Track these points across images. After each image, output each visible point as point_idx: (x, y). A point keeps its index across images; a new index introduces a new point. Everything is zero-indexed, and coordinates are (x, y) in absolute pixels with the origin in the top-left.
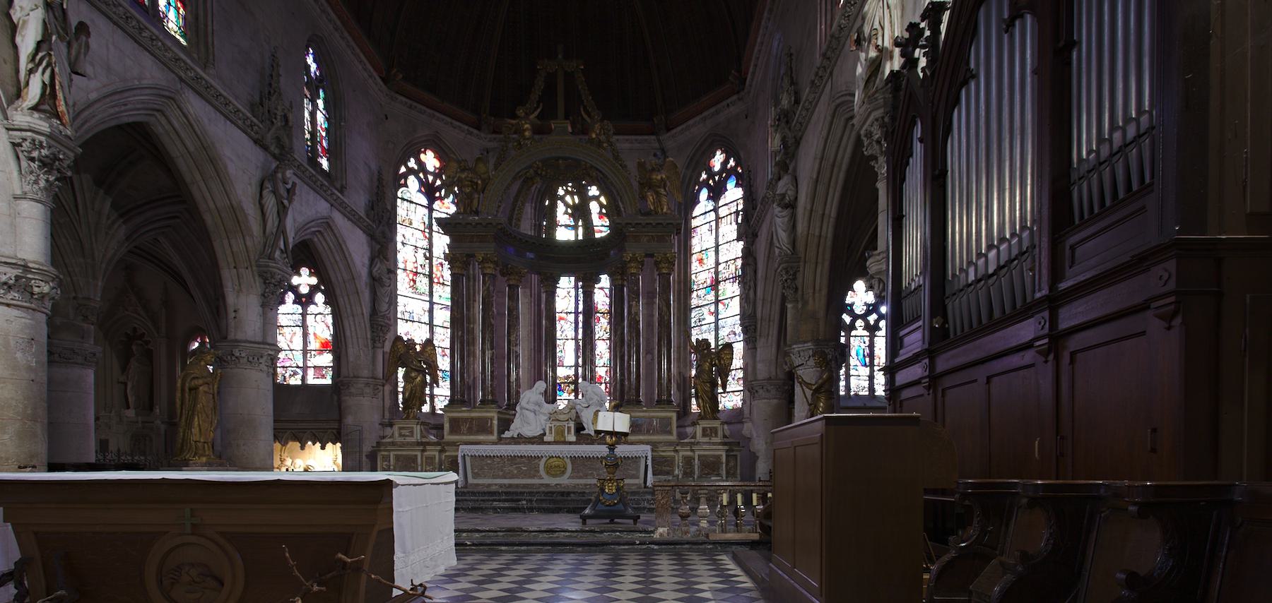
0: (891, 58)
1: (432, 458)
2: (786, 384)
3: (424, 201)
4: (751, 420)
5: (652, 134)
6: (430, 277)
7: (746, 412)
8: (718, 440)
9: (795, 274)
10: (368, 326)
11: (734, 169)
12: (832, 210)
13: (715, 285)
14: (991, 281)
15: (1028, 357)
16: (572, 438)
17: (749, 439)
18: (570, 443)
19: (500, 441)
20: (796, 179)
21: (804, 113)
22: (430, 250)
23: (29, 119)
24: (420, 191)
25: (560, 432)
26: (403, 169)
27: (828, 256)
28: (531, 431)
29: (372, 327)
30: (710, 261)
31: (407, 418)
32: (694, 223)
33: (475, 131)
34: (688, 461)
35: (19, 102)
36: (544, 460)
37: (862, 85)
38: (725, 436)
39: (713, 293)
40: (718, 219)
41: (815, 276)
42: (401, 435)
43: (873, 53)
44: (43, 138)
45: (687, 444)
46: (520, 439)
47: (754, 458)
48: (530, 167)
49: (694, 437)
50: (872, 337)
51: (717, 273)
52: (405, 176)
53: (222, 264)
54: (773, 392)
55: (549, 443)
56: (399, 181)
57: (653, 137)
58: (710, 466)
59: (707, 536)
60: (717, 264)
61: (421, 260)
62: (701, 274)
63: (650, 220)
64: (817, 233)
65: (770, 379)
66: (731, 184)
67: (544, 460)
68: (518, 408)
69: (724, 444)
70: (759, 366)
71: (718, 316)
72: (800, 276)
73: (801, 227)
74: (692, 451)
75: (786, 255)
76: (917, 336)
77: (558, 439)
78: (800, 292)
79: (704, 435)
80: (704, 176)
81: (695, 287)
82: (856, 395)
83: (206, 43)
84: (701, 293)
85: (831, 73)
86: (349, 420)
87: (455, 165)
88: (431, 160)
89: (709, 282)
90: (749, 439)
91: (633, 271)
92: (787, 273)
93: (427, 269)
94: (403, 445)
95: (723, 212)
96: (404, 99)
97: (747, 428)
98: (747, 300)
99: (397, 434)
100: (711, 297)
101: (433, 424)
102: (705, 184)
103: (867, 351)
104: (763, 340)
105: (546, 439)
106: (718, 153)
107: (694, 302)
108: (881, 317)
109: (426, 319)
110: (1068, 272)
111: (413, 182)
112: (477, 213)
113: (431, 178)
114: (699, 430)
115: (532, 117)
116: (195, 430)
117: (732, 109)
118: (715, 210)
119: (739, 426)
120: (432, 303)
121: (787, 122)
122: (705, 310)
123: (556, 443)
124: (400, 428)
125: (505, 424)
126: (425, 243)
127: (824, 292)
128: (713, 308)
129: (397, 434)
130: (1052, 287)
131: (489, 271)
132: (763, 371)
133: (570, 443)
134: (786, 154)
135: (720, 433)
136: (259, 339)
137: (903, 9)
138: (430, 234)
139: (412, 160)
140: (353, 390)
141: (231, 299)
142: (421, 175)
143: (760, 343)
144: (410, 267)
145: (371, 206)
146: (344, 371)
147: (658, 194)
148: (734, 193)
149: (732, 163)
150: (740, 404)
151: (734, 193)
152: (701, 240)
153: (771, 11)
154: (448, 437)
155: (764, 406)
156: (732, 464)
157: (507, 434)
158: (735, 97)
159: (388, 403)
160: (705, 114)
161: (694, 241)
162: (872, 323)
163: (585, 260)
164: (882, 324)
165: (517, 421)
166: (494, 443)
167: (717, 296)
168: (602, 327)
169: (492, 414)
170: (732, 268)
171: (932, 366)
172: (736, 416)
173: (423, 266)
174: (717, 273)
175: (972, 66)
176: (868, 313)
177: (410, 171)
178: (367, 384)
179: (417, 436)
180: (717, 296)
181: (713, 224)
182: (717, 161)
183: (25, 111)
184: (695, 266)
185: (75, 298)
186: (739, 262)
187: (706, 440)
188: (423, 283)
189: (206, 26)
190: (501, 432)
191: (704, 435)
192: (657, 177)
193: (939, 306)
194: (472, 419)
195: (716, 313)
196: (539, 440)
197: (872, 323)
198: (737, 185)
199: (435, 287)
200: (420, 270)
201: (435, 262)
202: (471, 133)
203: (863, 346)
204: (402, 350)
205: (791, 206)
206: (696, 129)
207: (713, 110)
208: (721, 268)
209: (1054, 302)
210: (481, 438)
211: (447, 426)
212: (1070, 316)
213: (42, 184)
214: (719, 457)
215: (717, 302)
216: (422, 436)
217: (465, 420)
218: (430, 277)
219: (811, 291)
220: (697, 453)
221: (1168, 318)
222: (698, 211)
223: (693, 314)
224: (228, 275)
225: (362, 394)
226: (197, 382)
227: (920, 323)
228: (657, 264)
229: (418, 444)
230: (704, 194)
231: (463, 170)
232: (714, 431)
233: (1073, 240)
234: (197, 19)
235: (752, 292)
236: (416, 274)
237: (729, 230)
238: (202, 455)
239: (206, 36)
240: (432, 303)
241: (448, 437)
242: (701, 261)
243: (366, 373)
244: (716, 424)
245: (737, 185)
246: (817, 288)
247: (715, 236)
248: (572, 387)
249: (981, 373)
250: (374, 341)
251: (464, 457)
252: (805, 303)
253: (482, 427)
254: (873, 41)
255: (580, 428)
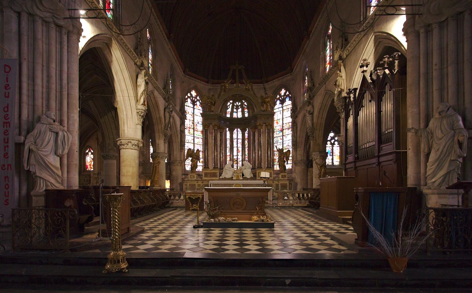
0: (344, 91)
1: (200, 185)
2: (309, 164)
3: (192, 106)
4: (295, 172)
5: (261, 83)
6: (194, 129)
7: (293, 170)
8: (286, 179)
9: (313, 133)
10: (179, 145)
11: (288, 95)
12: (325, 116)
13: (282, 130)
14: (368, 149)
15: (374, 165)
16: (241, 178)
17: (295, 178)
18: (241, 180)
19: (220, 179)
20: (313, 106)
21: (316, 90)
22: (194, 121)
23: (141, 107)
24: (191, 103)
25: (238, 176)
26: (186, 97)
27: (323, 129)
28: (229, 176)
29: (180, 145)
30: (280, 123)
31: (192, 173)
32: (275, 111)
33: (207, 84)
34: (277, 185)
35: (138, 103)
36: (234, 185)
37: (337, 96)
38: (288, 178)
39: (281, 133)
40: (283, 110)
41: (319, 133)
42: (190, 178)
43: (339, 90)
44: (143, 111)
45: (276, 180)
46: (225, 179)
47: (296, 184)
48: (228, 97)
49: (279, 178)
50: (333, 147)
51: (283, 127)
52: (187, 99)
53: (156, 132)
54: (303, 164)
55: (234, 180)
56: (185, 100)
57: (262, 84)
58: (284, 186)
59: (293, 205)
60: (283, 124)
61: (191, 124)
62: (277, 127)
63: (265, 113)
64: (320, 122)
65: (301, 160)
66: (287, 100)
67: (234, 185)
68: (224, 169)
69: (288, 180)
70: (298, 156)
71: (284, 139)
72: (314, 133)
73: (315, 120)
74: (279, 182)
75: (311, 127)
76: (352, 157)
77: (237, 179)
78: (314, 138)
79: (282, 177)
80: (278, 96)
81: (275, 131)
82: (328, 165)
83: (156, 75)
84: (278, 133)
85: (325, 83)
86: (174, 173)
87: (206, 97)
88: (194, 93)
89: (280, 130)
90: (295, 178)
91: (260, 128)
92: (311, 132)
93: (193, 127)
94: (192, 181)
95: (284, 108)
96: (188, 76)
97: (294, 175)
98: (294, 136)
99: (189, 177)
100: (281, 134)
101: (199, 175)
102: (279, 99)
103: (331, 151)
104: (299, 149)
105: (233, 179)
106: (283, 89)
107: (275, 135)
108: (335, 141)
109: (192, 142)
110: (381, 151)
111: (189, 100)
112: (213, 112)
113: (194, 99)
114: (280, 176)
115: (229, 82)
116: (156, 178)
117: (288, 77)
118: (282, 107)
119: (291, 174)
120: (194, 137)
121: (311, 91)
122: (279, 138)
123: (237, 180)
124: (191, 176)
125: (220, 175)
126: (192, 119)
127: (322, 138)
128: (281, 138)
129: (189, 177)
130: (378, 154)
131: (216, 129)
132: (299, 158)
133: (241, 180)
134: (310, 99)
135: (287, 177)
136: (163, 152)
137: (346, 80)
138: (194, 116)
139: (189, 94)
140: (175, 165)
141: (157, 141)
142: (191, 98)
143: (298, 149)
144: (188, 126)
145: (180, 110)
146: (172, 159)
147: (267, 105)
148: (288, 102)
149: (288, 93)
150: (291, 168)
151: (288, 102)
152: (277, 116)
153: (303, 54)
154: (204, 178)
155: (298, 169)
156: (290, 186)
157: (221, 177)
158: (289, 74)
159: (183, 168)
160: (279, 78)
161: (275, 117)
162: (333, 142)
163: (241, 123)
164: (336, 143)
165: (223, 173)
166: (218, 180)
167: (283, 134)
168: (246, 142)
169: (217, 172)
170: (288, 125)
171: (355, 165)
172: (290, 171)
173: (192, 126)
174: (283, 127)
175: (363, 105)
176: (331, 139)
177: (188, 97)
178: (179, 163)
179: (195, 178)
180: (283, 134)
181: (282, 111)
182: (283, 92)
183: (141, 105)
184: (275, 124)
185: (114, 141)
186: (290, 124)
187: (283, 179)
188: (192, 131)
189: (156, 71)
190: (219, 177)
191: (282, 177)
192: (267, 100)
193: (356, 152)
194: (211, 173)
195: (283, 139)
196: (231, 179)
197: (333, 142)
198: (289, 100)
199: (195, 132)
200: (191, 127)
201: (195, 124)
202: (205, 85)
203: (330, 150)
204: (190, 152)
205: (312, 114)
206: (276, 83)
207: (282, 77)
208: (284, 125)
209: (379, 156)
210: (214, 178)
211: (204, 175)
212: (382, 159)
213: (142, 121)
214: (286, 184)
215: (283, 136)
216: (197, 178)
217: (209, 173)
218: (194, 129)
219: (318, 138)
220: (280, 183)
221: (395, 163)
222: (276, 107)
223: (275, 139)
224: (157, 135)
225: (178, 165)
226: (156, 165)
227: (352, 155)
228: (266, 126)
229: (196, 180)
230: (278, 102)
231: (208, 99)
232: (285, 176)
233: (382, 146)
234: (154, 69)
235: (296, 135)
236: (190, 128)
237: (288, 113)
238: (157, 184)
239: (156, 73)
240: (194, 137)
241: (204, 178)
242: (277, 123)
243: (179, 159)
244: (285, 174)
245: (289, 100)
246: (320, 137)
247: (283, 115)
248: (236, 162)
249: (366, 167)
250: (181, 149)
251: (210, 184)
252: (316, 141)
253: (214, 175)
254: (339, 87)
255: (243, 175)
